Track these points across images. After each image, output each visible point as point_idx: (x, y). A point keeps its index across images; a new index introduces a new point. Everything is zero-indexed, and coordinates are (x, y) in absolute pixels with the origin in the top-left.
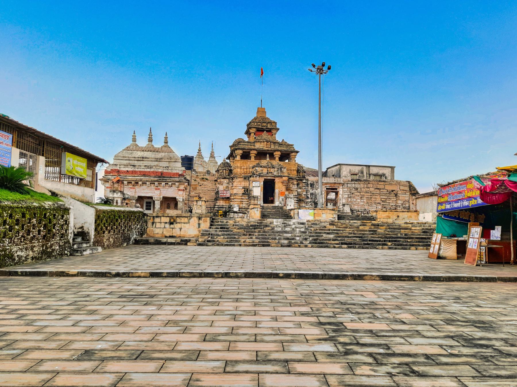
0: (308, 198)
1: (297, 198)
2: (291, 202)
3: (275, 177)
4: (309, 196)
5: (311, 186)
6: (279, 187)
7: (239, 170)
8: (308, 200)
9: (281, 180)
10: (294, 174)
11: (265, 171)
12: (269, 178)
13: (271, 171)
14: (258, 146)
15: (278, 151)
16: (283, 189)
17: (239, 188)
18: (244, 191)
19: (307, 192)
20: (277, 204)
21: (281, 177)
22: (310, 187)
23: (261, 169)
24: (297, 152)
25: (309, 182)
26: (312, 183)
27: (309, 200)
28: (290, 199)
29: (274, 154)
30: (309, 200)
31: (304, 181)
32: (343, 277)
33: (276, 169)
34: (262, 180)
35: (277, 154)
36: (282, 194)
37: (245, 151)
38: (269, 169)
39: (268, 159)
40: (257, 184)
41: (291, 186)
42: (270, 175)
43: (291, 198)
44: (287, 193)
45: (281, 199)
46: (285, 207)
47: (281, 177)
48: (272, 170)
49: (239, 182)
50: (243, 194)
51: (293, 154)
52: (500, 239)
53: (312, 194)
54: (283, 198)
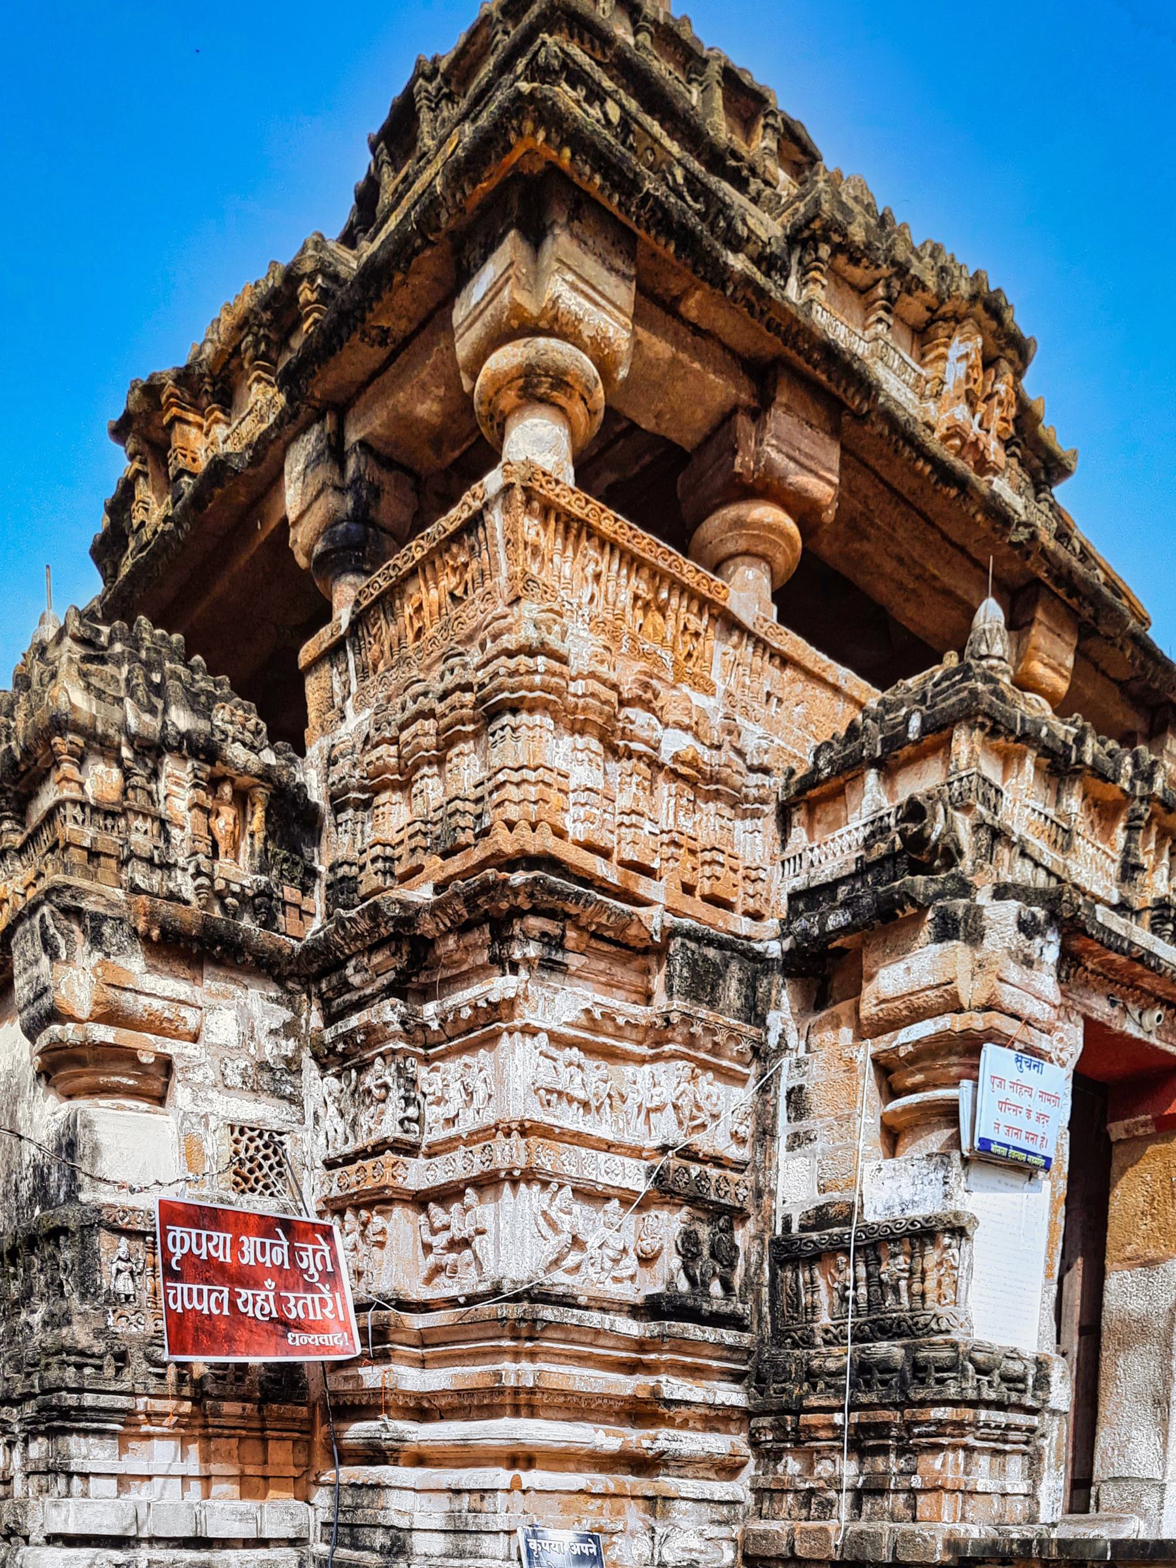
49: (596, 1042)
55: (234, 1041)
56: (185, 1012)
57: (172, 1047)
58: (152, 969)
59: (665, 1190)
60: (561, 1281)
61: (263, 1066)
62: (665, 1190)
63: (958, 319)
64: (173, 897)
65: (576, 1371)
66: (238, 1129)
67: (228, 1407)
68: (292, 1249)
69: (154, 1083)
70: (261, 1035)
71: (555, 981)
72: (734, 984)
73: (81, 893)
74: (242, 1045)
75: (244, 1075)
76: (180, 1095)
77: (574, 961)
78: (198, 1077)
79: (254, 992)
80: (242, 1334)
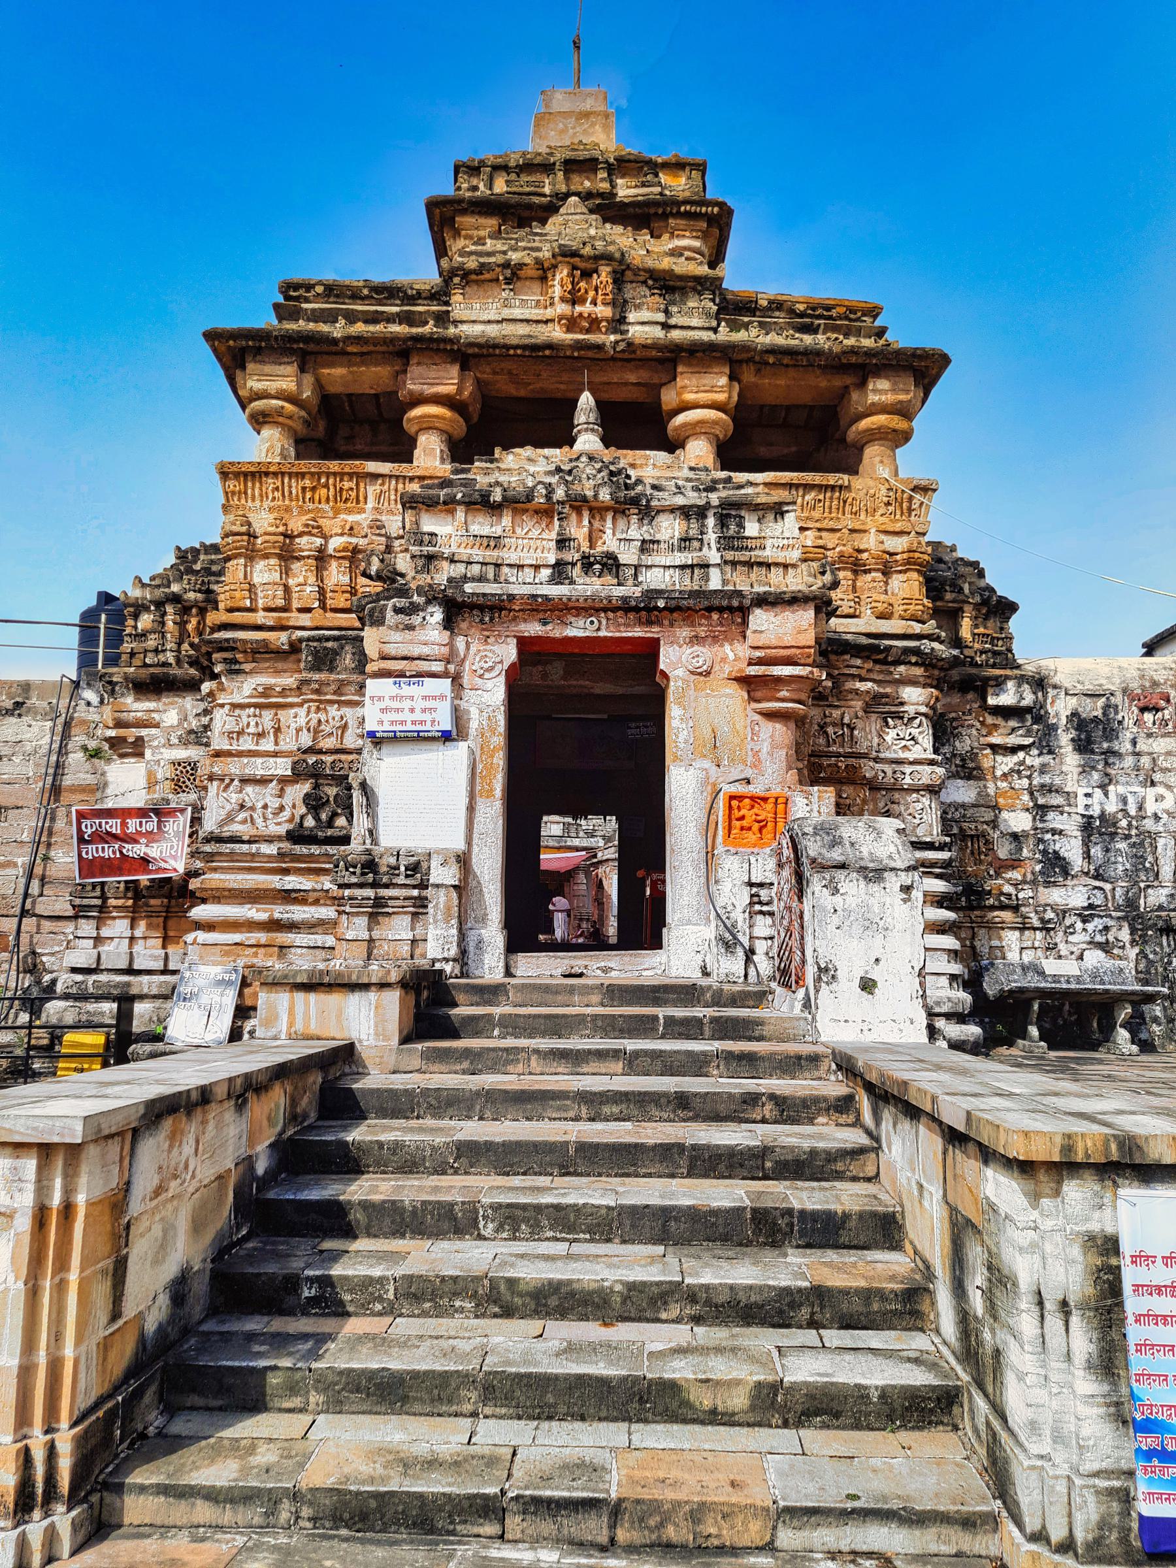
0: (1055, 867)
1: (945, 871)
2: (872, 925)
3: (647, 609)
4: (1071, 849)
5: (1083, 746)
6: (714, 734)
7: (264, 573)
8: (1055, 895)
9: (734, 655)
10: (886, 606)
11: (530, 546)
12: (579, 628)
13: (609, 542)
14: (479, 317)
15: (700, 355)
16: (765, 754)
17: (259, 767)
18: (314, 803)
19: (1041, 811)
20: (686, 949)
21: (732, 611)
22: (1071, 760)
23: (482, 525)
24: (924, 368)
25: (1060, 709)
26: (1094, 709)
27: (1074, 896)
28: (852, 888)
29: (669, 398)
30: (1074, 896)
31: (1007, 698)
32: (521, 321)
33: (669, 528)
34: (491, 658)
35: (701, 397)
36: (743, 815)
37: (336, 374)
38: (578, 530)
39: (588, 441)
40: (426, 705)
41: (868, 734)
42: (588, 586)
43: (874, 874)
44: (812, 806)
45: (733, 896)
46: (784, 1006)
47: (732, 611)
48: (619, 538)
49: (266, 701)
50: (297, 836)
51: (881, 391)
52: (545, 818)
53: (1096, 829)
54: (764, 867)
55: (176, 723)
56: (154, 715)
57: (144, 732)
58: (137, 700)
59: (298, 775)
60: (236, 828)
61: (191, 732)
62: (298, 775)
63: (555, 267)
64: (165, 664)
65: (232, 877)
66: (176, 764)
67: (153, 902)
68: (159, 822)
69: (137, 749)
70: (190, 718)
71: (241, 678)
72: (349, 656)
73: (111, 675)
74: (180, 723)
75: (180, 738)
76: (148, 753)
77: (247, 667)
78: (156, 743)
79: (189, 699)
80: (126, 866)
